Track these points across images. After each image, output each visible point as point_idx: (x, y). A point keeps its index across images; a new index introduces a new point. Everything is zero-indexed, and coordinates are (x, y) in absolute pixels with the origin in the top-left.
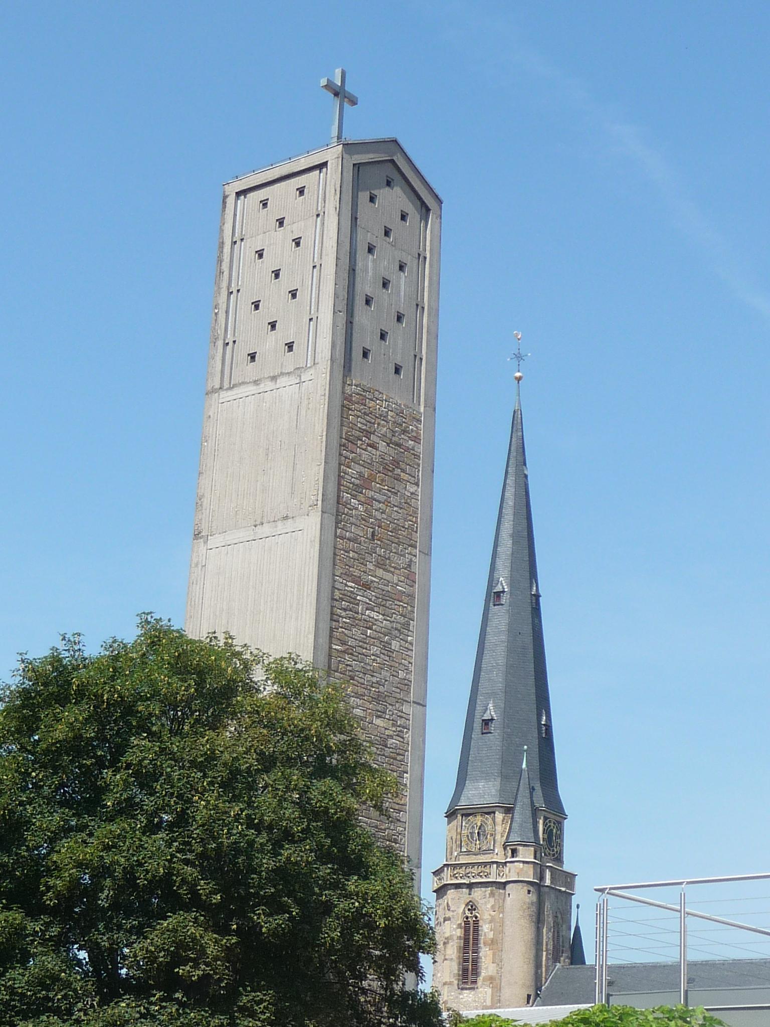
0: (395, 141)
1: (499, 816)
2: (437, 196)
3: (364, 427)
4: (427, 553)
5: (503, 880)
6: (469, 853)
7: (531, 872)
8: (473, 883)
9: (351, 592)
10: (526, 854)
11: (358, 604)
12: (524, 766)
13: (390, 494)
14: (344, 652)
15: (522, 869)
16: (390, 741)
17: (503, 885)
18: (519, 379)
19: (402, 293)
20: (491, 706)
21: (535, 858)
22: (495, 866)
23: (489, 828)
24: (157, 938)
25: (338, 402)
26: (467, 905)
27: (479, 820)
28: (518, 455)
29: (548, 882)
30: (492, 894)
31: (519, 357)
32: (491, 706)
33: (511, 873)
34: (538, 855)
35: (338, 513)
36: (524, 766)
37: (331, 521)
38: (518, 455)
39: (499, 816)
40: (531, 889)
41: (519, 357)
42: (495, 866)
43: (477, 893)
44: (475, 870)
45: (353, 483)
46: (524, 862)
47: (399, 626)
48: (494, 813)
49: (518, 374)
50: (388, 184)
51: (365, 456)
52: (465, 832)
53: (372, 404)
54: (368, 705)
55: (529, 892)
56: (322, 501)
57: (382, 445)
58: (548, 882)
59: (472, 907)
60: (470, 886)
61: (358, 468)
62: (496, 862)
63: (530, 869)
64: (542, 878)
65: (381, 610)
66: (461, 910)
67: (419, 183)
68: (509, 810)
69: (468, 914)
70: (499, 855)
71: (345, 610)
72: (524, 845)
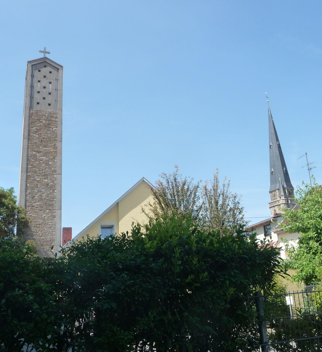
0: (46, 57)
1: (277, 191)
2: (61, 66)
3: (38, 119)
4: (61, 141)
5: (280, 204)
6: (273, 200)
7: (284, 201)
8: (274, 206)
9: (34, 154)
10: (283, 198)
11: (37, 156)
12: (280, 180)
13: (47, 131)
14: (33, 167)
15: (282, 201)
16: (49, 184)
17: (280, 205)
18: (268, 102)
19: (50, 88)
20: (272, 169)
21: (285, 198)
22: (277, 201)
23: (276, 194)
24: (318, 226)
25: (27, 115)
26: (274, 210)
27: (273, 193)
28: (271, 117)
29: (290, 202)
30: (278, 207)
31: (267, 97)
32: (272, 169)
33: (281, 202)
34: (286, 197)
35: (28, 138)
36: (280, 180)
37: (26, 141)
38: (271, 117)
39: (277, 191)
40: (285, 204)
41: (267, 97)
42: (277, 201)
43: (275, 207)
44: (274, 203)
45: (34, 131)
46: (282, 199)
47: (51, 159)
48: (276, 191)
49: (267, 101)
50: (45, 67)
51: (38, 125)
52: (272, 196)
53: (40, 113)
54: (41, 177)
55: (285, 205)
56: (23, 137)
57: (44, 121)
58: (290, 202)
59: (275, 211)
60: (274, 206)
61: (35, 128)
62: (278, 201)
63: (284, 201)
64: (288, 202)
65: (45, 156)
66: (273, 212)
67: (56, 65)
68: (278, 189)
69: (275, 212)
70: (278, 199)
71: (33, 158)
72: (282, 196)
